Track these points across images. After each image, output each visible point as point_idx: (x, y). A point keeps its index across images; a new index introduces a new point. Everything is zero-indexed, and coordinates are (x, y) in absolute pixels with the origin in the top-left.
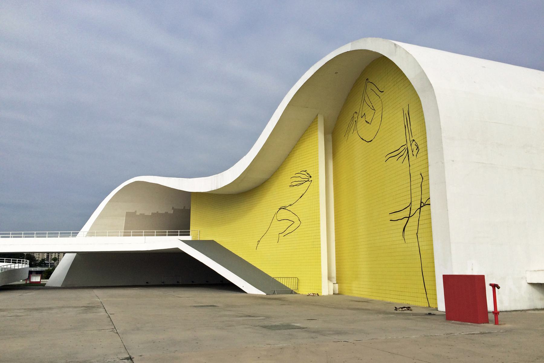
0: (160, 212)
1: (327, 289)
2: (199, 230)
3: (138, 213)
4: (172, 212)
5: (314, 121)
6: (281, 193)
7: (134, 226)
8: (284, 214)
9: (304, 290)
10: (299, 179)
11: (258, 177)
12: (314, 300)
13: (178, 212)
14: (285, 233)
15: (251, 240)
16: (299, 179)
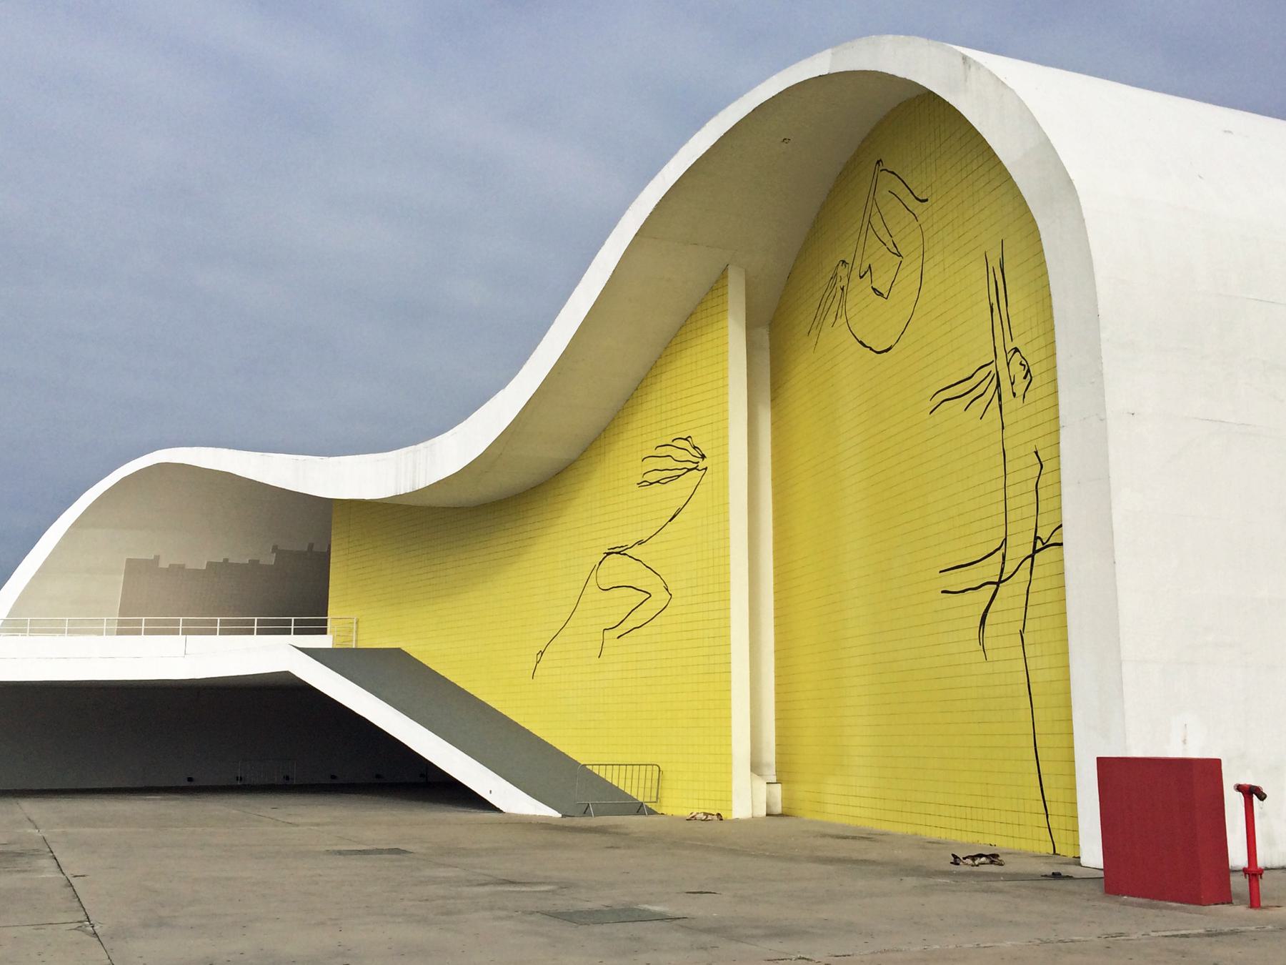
0: (234, 560)
1: (747, 800)
2: (356, 617)
3: (164, 564)
4: (270, 560)
5: (718, 285)
6: (611, 503)
7: (156, 599)
8: (618, 569)
9: (679, 803)
10: (669, 463)
11: (542, 453)
12: (709, 836)
13: (292, 563)
14: (621, 629)
15: (512, 647)
16: (669, 463)
